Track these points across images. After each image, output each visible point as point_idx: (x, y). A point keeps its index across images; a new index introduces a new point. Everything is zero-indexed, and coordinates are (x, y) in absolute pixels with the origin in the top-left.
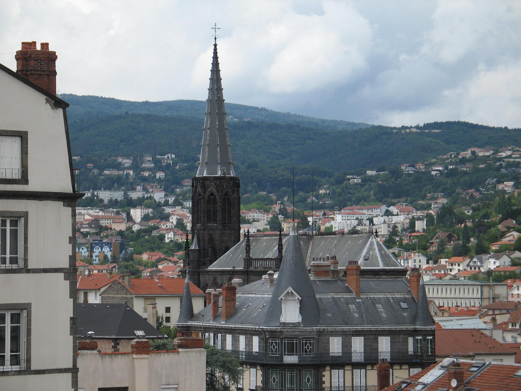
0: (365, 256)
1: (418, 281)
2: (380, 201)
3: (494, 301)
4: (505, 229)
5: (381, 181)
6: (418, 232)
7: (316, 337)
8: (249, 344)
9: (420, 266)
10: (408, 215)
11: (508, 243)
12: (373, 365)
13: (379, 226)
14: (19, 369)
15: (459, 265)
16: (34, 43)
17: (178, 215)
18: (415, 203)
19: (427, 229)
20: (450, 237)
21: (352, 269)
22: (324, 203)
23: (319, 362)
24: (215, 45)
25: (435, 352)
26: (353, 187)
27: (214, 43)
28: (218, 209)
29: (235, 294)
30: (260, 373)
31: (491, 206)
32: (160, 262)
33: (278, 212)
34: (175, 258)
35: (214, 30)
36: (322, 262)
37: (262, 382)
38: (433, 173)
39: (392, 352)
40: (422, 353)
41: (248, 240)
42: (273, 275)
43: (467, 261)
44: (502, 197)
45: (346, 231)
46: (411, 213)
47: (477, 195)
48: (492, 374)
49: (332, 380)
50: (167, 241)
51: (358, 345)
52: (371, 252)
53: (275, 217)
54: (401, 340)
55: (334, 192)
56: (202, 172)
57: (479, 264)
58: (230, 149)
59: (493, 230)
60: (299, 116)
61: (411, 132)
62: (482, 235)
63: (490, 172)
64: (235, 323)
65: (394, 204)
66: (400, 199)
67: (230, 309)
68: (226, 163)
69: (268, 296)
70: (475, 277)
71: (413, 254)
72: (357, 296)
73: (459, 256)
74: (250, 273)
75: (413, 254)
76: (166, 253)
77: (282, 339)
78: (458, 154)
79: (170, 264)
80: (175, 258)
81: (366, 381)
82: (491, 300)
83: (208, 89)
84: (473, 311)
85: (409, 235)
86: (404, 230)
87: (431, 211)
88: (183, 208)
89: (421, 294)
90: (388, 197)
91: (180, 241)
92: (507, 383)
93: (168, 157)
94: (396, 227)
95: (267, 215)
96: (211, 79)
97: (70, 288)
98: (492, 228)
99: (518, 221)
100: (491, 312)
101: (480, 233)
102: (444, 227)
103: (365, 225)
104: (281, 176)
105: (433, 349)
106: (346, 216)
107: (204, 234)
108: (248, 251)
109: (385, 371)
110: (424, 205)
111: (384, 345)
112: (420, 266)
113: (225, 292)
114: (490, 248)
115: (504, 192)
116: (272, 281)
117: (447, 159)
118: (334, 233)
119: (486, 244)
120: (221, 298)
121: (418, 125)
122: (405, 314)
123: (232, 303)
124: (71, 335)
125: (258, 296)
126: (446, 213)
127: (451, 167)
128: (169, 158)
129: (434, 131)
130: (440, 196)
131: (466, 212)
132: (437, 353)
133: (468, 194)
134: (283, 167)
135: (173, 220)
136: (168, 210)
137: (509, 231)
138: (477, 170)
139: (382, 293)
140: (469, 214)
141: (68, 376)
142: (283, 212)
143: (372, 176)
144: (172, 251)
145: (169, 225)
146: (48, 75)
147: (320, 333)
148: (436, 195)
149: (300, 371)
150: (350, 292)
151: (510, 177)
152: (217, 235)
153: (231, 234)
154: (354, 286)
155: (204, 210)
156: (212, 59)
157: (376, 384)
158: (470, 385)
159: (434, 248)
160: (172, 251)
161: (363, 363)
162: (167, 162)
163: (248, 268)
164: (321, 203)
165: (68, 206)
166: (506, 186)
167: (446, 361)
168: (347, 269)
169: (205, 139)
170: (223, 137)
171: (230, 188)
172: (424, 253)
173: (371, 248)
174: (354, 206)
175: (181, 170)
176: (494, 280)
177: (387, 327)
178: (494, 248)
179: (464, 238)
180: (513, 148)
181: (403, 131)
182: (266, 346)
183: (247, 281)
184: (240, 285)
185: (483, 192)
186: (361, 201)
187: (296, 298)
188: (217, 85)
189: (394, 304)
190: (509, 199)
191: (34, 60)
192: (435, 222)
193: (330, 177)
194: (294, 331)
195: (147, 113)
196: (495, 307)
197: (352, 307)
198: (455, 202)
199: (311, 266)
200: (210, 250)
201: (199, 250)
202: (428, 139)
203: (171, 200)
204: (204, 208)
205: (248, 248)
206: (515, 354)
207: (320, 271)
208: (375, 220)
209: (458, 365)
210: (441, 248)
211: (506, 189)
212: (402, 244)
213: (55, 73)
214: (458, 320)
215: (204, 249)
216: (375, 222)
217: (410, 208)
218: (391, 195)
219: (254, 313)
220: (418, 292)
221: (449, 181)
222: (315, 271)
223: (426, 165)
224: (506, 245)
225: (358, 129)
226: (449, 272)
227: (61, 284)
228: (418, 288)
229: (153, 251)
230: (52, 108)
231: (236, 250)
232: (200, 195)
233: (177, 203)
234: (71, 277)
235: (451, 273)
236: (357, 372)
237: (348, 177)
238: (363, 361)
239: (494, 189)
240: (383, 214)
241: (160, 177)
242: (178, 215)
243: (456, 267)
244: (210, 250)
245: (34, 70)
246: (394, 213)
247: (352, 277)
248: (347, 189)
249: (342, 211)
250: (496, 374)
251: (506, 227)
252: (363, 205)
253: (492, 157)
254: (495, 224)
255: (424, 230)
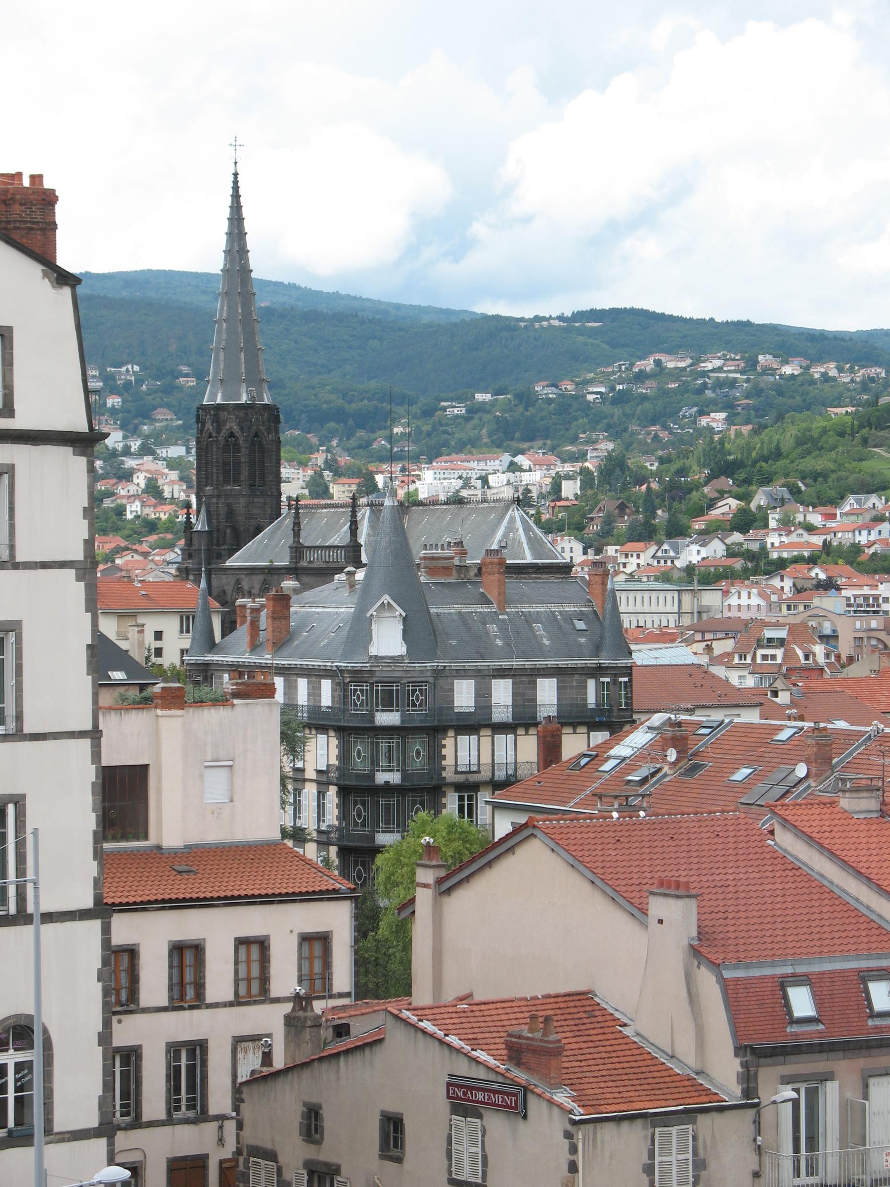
0: (500, 541)
1: (604, 584)
2: (499, 447)
3: (700, 617)
4: (716, 495)
5: (501, 411)
6: (567, 499)
7: (431, 680)
8: (314, 692)
9: (571, 558)
10: (548, 470)
11: (721, 518)
12: (527, 727)
13: (499, 490)
14: (4, 732)
15: (638, 556)
16: (20, 175)
17: (147, 471)
18: (559, 449)
19: (584, 495)
20: (622, 508)
21: (491, 564)
22: (402, 451)
23: (436, 724)
24: (236, 175)
25: (632, 704)
26: (451, 422)
27: (234, 171)
28: (243, 460)
29: (288, 607)
30: (334, 742)
31: (691, 454)
32: (118, 552)
33: (323, 466)
34: (145, 547)
35: (233, 148)
36: (440, 551)
37: (338, 757)
38: (590, 397)
39: (559, 705)
40: (611, 705)
41: (297, 515)
42: (353, 573)
43: (654, 548)
44: (708, 439)
45: (442, 498)
46: (552, 467)
47: (664, 436)
48: (735, 738)
49: (458, 754)
50: (129, 516)
51: (502, 693)
52: (511, 535)
53: (319, 475)
54: (575, 684)
55: (419, 431)
56: (213, 396)
57: (672, 554)
58: (262, 356)
59: (695, 495)
60: (355, 298)
61: (551, 327)
62: (676, 504)
63: (686, 395)
64: (290, 657)
65: (522, 452)
66: (534, 444)
67: (280, 632)
68: (255, 380)
69: (347, 610)
70: (665, 577)
71: (559, 538)
72: (499, 609)
73: (638, 541)
74: (310, 568)
75: (559, 538)
76: (127, 537)
77: (372, 684)
78: (632, 365)
79: (137, 557)
80: (145, 547)
81: (516, 755)
82: (696, 615)
83: (224, 251)
84: (669, 634)
85: (552, 504)
86: (542, 496)
87: (587, 464)
88: (155, 459)
89: (610, 606)
90: (512, 439)
91: (153, 516)
92: (761, 754)
93: (127, 370)
94: (529, 491)
95: (304, 470)
96: (229, 234)
97: (86, 595)
98: (694, 493)
99: (737, 480)
100: (698, 637)
101: (674, 500)
102: (610, 490)
103: (475, 488)
104: (326, 402)
105: (629, 699)
106: (442, 472)
107: (217, 503)
108: (297, 533)
109: (553, 736)
110: (574, 453)
111: (547, 693)
112: (571, 558)
113: (271, 603)
114: (690, 527)
115: (711, 430)
116: (352, 585)
117: (613, 373)
118: (421, 504)
119: (684, 519)
120: (264, 614)
121: (563, 314)
122: (583, 640)
123: (284, 622)
124: (88, 674)
125: (328, 610)
126: (614, 467)
127: (621, 387)
128: (130, 371)
129: (590, 324)
130: (601, 437)
131: (648, 464)
132: (635, 707)
133: (649, 433)
134: (329, 387)
135: (140, 480)
136: (130, 463)
137: (722, 498)
138: (666, 393)
139: (540, 604)
140: (654, 468)
141: (85, 744)
142: (331, 465)
143: (484, 403)
144: (139, 534)
145: (132, 489)
146: (42, 229)
147: (438, 673)
148: (594, 437)
149: (403, 738)
150: (488, 602)
151: (720, 405)
152: (240, 505)
153: (265, 504)
154: (495, 592)
155: (217, 462)
156: (230, 198)
157: (536, 760)
158: (698, 758)
159: (595, 527)
160: (139, 534)
161: (511, 724)
162: (126, 379)
163: (297, 562)
164: (396, 449)
165: (82, 454)
166: (714, 420)
167: (658, 719)
168: (483, 563)
169: (217, 339)
170: (250, 336)
171: (263, 425)
172: (579, 536)
173: (511, 528)
174: (454, 456)
175: (150, 392)
176: (699, 583)
177: (551, 663)
178: (697, 527)
179: (646, 510)
180: (724, 355)
181: (537, 325)
182: (345, 697)
183: (305, 587)
184: (296, 591)
185: (675, 431)
186: (467, 446)
187: (397, 613)
188: (239, 244)
189: (562, 623)
190: (722, 442)
191: (21, 204)
192: (596, 482)
193: (410, 405)
194: (393, 670)
195: (89, 292)
196: (706, 627)
197: (493, 628)
198: (628, 447)
199: (421, 559)
200: (228, 531)
201: (209, 533)
202: (580, 339)
203: (135, 445)
204: (217, 459)
205: (296, 528)
206: (761, 705)
207: (436, 566)
208: (491, 478)
209: (679, 724)
210: (607, 527)
211: (714, 425)
212: (540, 520)
213: (53, 226)
214: (650, 650)
215: (218, 530)
216: (491, 484)
217: (553, 458)
218: (517, 435)
219: (322, 641)
220: (603, 602)
221: (617, 411)
222: (427, 567)
223: (577, 384)
224: (718, 521)
225: (458, 321)
226: (621, 569)
227: (70, 589)
228: (603, 595)
229: (104, 535)
230: (53, 287)
231: (273, 532)
232: (211, 437)
233: (146, 450)
234: (87, 577)
235: (624, 570)
236: (500, 738)
237: (443, 404)
238: (510, 720)
239: (694, 426)
240: (505, 469)
241: (113, 405)
242: (147, 471)
243: (633, 562)
244: (228, 531)
245: (19, 221)
246: (524, 468)
247: (490, 577)
248: (441, 426)
249: (434, 464)
250: (742, 739)
251: (717, 491)
252: (470, 453)
253: (691, 371)
254: (697, 487)
255: (577, 497)
